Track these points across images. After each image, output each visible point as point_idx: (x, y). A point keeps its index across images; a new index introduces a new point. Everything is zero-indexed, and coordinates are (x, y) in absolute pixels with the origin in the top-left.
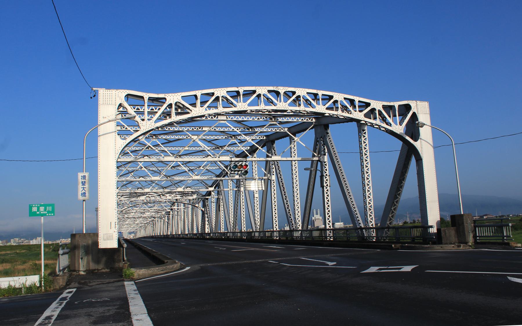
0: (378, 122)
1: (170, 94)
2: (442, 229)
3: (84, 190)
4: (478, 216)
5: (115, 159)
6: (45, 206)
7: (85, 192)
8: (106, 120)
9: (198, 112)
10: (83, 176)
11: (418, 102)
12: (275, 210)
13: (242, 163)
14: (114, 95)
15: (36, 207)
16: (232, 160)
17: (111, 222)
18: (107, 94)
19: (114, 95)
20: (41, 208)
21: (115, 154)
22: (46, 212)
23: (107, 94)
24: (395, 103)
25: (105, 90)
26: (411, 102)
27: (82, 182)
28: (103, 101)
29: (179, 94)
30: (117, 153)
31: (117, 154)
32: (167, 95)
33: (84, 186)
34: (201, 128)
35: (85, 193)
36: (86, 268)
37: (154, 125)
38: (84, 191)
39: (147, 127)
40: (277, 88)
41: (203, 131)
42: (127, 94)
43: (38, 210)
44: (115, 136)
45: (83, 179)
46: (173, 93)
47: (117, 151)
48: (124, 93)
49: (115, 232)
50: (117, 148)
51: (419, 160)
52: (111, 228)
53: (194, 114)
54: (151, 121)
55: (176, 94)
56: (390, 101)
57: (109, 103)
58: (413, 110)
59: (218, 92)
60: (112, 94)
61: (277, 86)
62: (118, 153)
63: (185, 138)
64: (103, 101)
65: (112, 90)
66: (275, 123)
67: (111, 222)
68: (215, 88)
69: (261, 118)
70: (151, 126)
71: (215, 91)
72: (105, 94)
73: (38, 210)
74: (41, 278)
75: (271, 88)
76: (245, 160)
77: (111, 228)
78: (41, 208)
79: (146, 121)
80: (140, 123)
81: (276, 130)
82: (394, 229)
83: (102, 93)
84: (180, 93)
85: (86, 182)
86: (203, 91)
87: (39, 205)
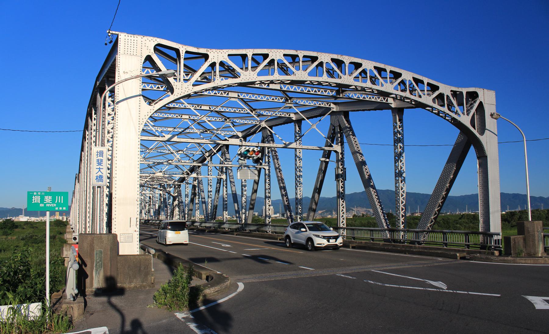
0: (445, 109)
1: (214, 50)
2: (512, 237)
3: (101, 172)
4: (420, 213)
5: (139, 130)
6: (54, 195)
7: (101, 174)
8: (127, 76)
9: (248, 77)
10: (99, 151)
11: (485, 90)
12: (343, 207)
13: (250, 148)
14: (139, 42)
15: (39, 195)
16: (243, 144)
17: (130, 218)
18: (133, 41)
19: (139, 42)
20: (46, 197)
21: (139, 124)
22: (55, 205)
23: (133, 41)
24: (463, 89)
25: (127, 35)
26: (479, 89)
27: (98, 160)
28: (125, 50)
29: (225, 51)
30: (141, 122)
31: (142, 124)
32: (210, 51)
33: (100, 166)
34: (200, 107)
35: (101, 177)
36: (102, 284)
37: (192, 89)
38: (100, 174)
39: (183, 91)
40: (342, 57)
41: (202, 110)
42: (158, 43)
43: (42, 200)
44: (140, 100)
45: (99, 155)
46: (220, 49)
47: (141, 120)
48: (154, 41)
49: (135, 231)
50: (142, 116)
51: (482, 156)
52: (130, 225)
53: (244, 80)
54: (189, 83)
55: (221, 51)
56: (458, 87)
57: (132, 53)
58: (481, 98)
59: (273, 54)
60: (137, 41)
61: (342, 54)
62: (143, 123)
63: (175, 117)
64: (125, 50)
65: (138, 36)
66: (290, 105)
67: (130, 218)
68: (270, 49)
69: (276, 99)
70: (188, 91)
71: (270, 52)
72: (128, 40)
73: (42, 200)
74: (44, 309)
75: (335, 56)
76: (258, 145)
77: (130, 225)
78: (46, 197)
79: (182, 83)
80: (174, 84)
81: (281, 114)
82: (441, 234)
83: (124, 38)
84: (227, 50)
85: (104, 161)
86: (255, 50)
87: (43, 194)
